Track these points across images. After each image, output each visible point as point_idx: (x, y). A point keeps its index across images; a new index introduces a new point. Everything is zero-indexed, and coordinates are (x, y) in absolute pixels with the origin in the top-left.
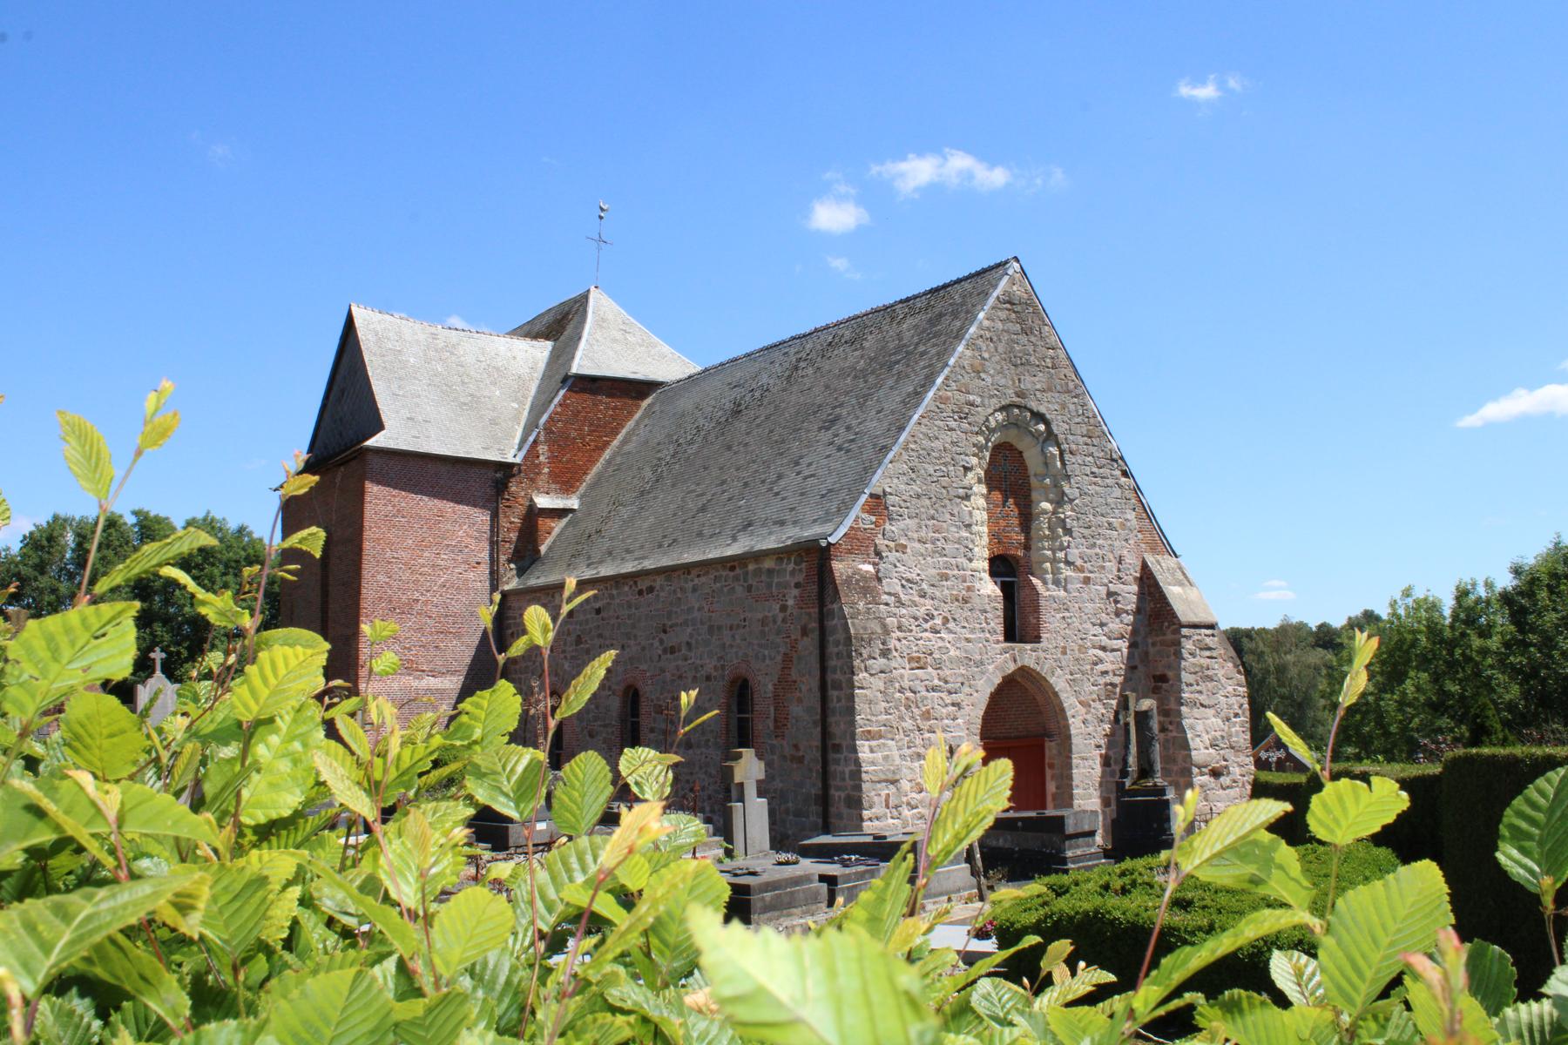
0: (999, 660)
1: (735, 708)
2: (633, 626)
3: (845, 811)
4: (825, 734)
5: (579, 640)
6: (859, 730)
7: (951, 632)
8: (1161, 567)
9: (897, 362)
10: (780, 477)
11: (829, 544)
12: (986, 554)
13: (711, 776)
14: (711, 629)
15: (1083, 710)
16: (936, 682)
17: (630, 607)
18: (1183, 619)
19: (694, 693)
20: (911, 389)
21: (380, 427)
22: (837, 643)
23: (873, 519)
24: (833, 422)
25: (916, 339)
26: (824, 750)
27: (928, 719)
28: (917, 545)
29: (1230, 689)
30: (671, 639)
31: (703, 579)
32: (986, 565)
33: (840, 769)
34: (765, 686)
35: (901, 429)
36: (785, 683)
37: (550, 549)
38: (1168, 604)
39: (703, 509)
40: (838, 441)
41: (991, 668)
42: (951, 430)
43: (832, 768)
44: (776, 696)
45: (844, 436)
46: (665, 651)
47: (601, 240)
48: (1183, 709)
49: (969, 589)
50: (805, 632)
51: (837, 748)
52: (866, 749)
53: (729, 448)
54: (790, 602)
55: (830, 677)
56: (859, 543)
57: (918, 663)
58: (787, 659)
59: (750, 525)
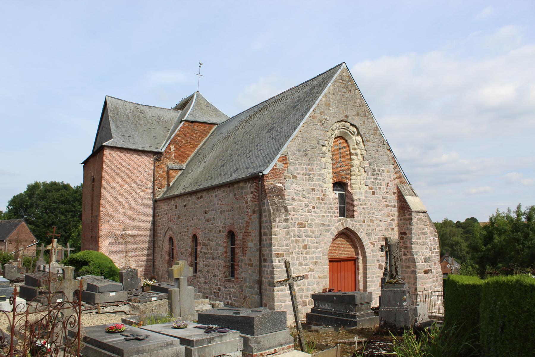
0: (337, 224)
1: (230, 244)
2: (196, 212)
3: (268, 287)
4: (261, 254)
5: (179, 217)
6: (273, 253)
7: (316, 213)
8: (405, 190)
9: (297, 105)
10: (250, 151)
11: (263, 174)
12: (332, 181)
13: (220, 271)
14: (221, 212)
15: (372, 246)
16: (309, 233)
17: (195, 204)
18: (413, 210)
19: (487, 267)
20: (301, 114)
21: (111, 138)
22: (266, 216)
23: (283, 165)
24: (272, 130)
25: (305, 96)
26: (260, 261)
27: (306, 249)
28: (301, 176)
29: (432, 238)
30: (208, 216)
31: (219, 192)
32: (331, 185)
33: (267, 269)
34: (239, 236)
35: (296, 128)
36: (247, 233)
37: (173, 184)
38: (407, 203)
39: (223, 166)
40: (272, 136)
41: (333, 228)
42: (317, 130)
43: (263, 269)
44: (243, 238)
45: (275, 133)
46: (206, 221)
47: (200, 75)
48: (412, 245)
49: (324, 195)
50: (254, 212)
51: (265, 260)
52: (277, 261)
53: (235, 143)
54: (249, 199)
55: (263, 231)
56: (277, 173)
57: (302, 225)
58: (248, 223)
59: (237, 170)
